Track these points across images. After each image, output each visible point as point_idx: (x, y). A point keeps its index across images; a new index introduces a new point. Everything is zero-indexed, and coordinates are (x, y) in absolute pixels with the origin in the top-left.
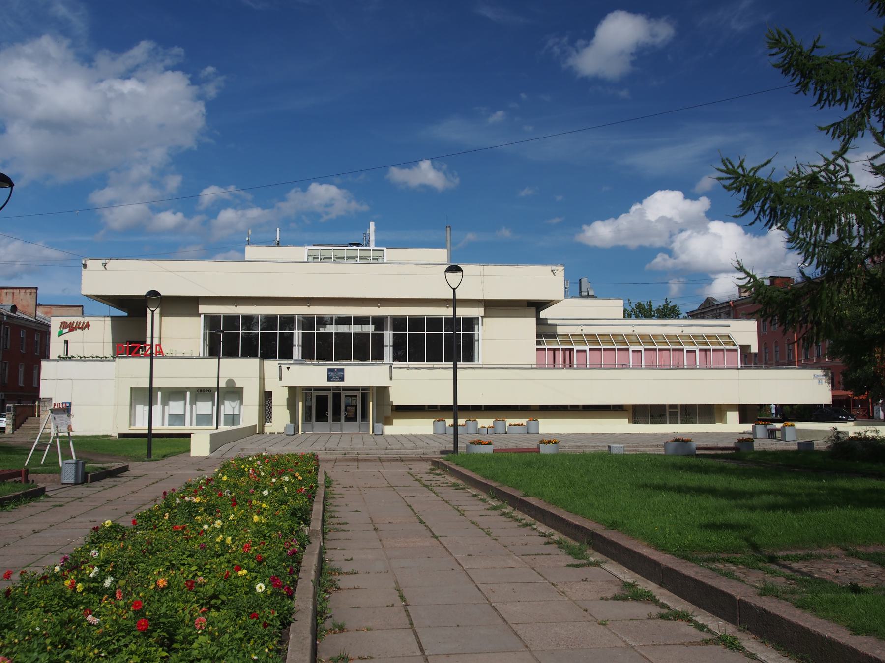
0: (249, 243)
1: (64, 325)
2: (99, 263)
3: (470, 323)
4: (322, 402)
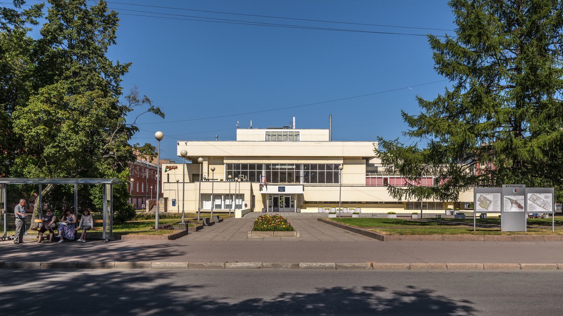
0: (238, 128)
1: (167, 167)
2: (184, 143)
3: (337, 166)
4: (276, 200)
